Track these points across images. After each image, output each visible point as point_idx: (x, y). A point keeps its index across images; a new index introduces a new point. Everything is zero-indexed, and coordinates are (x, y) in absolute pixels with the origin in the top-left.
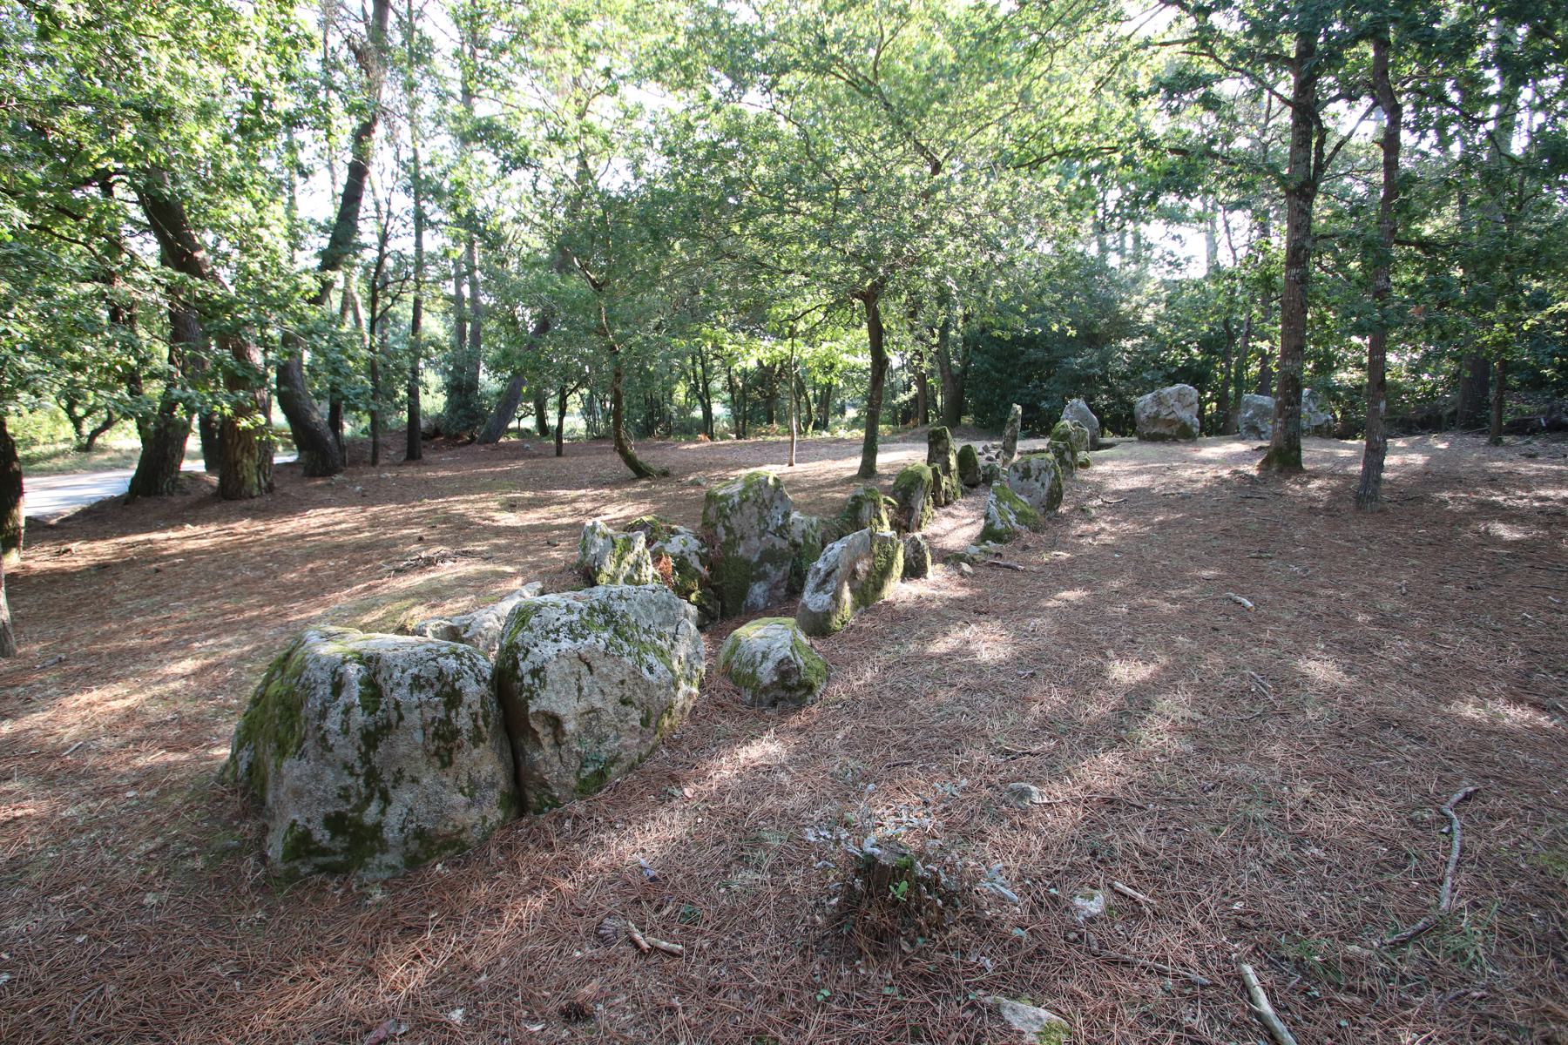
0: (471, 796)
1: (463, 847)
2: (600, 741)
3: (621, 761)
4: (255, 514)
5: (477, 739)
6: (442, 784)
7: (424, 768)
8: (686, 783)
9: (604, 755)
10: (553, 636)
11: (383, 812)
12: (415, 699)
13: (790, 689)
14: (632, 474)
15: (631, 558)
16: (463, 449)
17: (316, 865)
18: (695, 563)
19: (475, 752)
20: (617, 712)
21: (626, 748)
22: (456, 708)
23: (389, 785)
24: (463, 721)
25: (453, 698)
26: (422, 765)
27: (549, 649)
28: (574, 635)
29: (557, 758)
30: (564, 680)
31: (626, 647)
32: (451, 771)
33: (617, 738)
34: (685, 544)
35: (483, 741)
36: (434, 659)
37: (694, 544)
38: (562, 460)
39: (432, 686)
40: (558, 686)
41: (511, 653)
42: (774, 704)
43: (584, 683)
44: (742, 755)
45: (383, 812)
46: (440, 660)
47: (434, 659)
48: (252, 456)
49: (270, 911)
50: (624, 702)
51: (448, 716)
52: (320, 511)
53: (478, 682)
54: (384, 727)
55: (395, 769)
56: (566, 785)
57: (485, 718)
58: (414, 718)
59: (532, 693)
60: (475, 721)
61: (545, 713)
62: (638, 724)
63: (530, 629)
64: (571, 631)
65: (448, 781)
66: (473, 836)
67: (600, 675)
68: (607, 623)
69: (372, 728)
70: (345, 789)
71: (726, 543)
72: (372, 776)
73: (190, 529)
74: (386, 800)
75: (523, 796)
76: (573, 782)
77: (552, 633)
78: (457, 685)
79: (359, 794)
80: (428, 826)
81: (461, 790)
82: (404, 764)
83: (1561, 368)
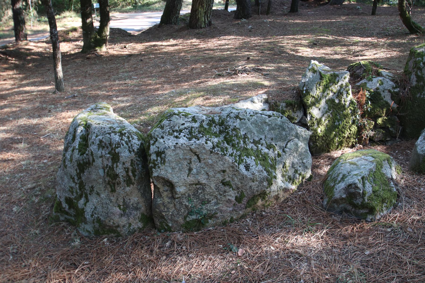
0: (124, 210)
1: (119, 235)
2: (204, 202)
3: (217, 218)
4: (199, 36)
5: (129, 182)
6: (110, 200)
7: (103, 189)
8: (245, 244)
9: (205, 212)
10: (175, 134)
11: (85, 204)
12: (99, 153)
13: (355, 206)
14: (407, 30)
15: (335, 88)
16: (322, 7)
17: (66, 218)
18: (387, 98)
19: (128, 189)
20: (218, 189)
21: (221, 211)
22: (117, 162)
23: (88, 192)
24: (120, 170)
25: (115, 157)
26: (102, 187)
27: (170, 142)
28: (191, 135)
29: (172, 205)
30: (178, 162)
31: (230, 150)
32: (115, 194)
33: (217, 204)
34: (382, 84)
35: (133, 184)
36: (109, 134)
37: (389, 84)
38: (375, 18)
39: (108, 147)
40: (173, 165)
41: (147, 140)
42: (341, 213)
43: (193, 166)
44: (292, 240)
45: (85, 204)
46: (113, 134)
47: (109, 134)
48: (203, 7)
49: (42, 231)
50: (224, 183)
51: (113, 166)
52: (226, 37)
53: (130, 152)
54: (87, 163)
55: (90, 185)
56: (177, 221)
57: (134, 171)
58: (99, 162)
59: (155, 165)
60: (127, 172)
61: (163, 179)
62: (233, 199)
63: (162, 128)
64: (190, 133)
65: (113, 199)
66: (124, 231)
67: (207, 164)
68: (221, 132)
69: (82, 162)
70: (72, 188)
71: (416, 87)
72: (82, 186)
73: (172, 42)
74: (87, 201)
75: (152, 219)
76: (181, 220)
77: (176, 132)
78: (117, 150)
79: (77, 193)
80: (102, 218)
81: (119, 206)
82: (94, 184)
83: (49, 9)
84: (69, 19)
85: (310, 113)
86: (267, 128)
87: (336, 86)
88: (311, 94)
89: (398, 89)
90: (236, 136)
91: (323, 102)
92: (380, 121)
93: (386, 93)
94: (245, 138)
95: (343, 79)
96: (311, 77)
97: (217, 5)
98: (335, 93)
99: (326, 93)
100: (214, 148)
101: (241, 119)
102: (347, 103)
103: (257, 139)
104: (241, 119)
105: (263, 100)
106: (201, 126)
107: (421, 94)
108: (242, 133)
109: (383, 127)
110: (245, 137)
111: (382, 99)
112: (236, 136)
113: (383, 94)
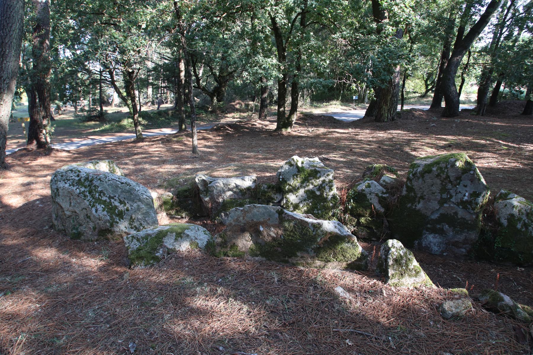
31: (89, 198)
33: (85, 228)
71: (406, 197)
84: (334, 106)
85: (286, 198)
86: (120, 190)
87: (318, 180)
88: (288, 182)
89: (388, 195)
90: (95, 190)
91: (301, 192)
92: (363, 220)
93: (373, 196)
94: (100, 193)
95: (325, 175)
96: (287, 168)
97: (464, 103)
98: (315, 186)
99: (305, 184)
100: (80, 194)
101: (101, 181)
102: (330, 197)
103: (112, 196)
104: (101, 181)
105: (252, 180)
106: (80, 180)
107: (412, 204)
108: (99, 189)
109: (367, 226)
110: (101, 192)
111: (368, 201)
112: (95, 190)
113: (369, 197)
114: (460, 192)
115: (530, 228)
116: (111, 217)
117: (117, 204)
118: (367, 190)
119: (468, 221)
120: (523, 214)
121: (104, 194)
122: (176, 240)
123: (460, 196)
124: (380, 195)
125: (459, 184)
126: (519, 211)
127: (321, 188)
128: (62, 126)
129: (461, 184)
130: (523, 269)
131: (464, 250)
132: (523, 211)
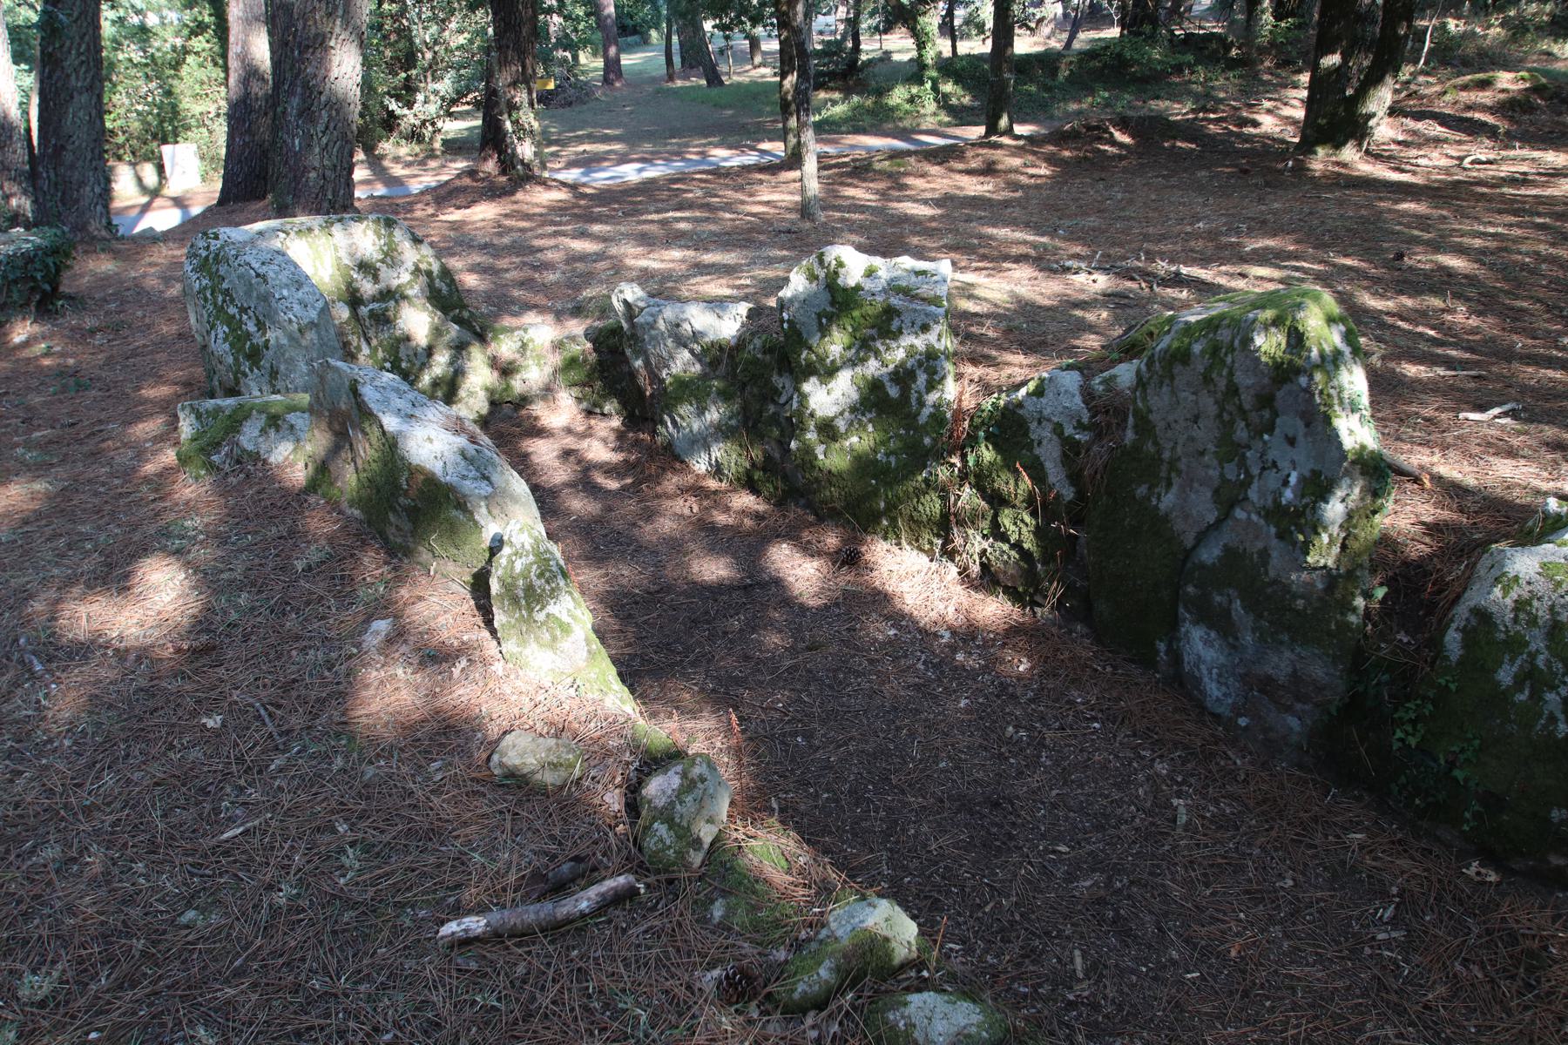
93: (1046, 432)
108: (225, 286)
110: (227, 292)
113: (1036, 432)
114: (1274, 464)
115: (1550, 696)
116: (236, 359)
117: (251, 327)
118: (1030, 406)
119: (1295, 596)
120: (1533, 621)
121: (232, 300)
122: (263, 431)
123: (1272, 479)
124: (1069, 431)
125: (1270, 429)
126: (1520, 605)
127: (903, 376)
128: (730, 107)
129: (1277, 431)
130: (1493, 877)
131: (1293, 722)
132: (1541, 610)
